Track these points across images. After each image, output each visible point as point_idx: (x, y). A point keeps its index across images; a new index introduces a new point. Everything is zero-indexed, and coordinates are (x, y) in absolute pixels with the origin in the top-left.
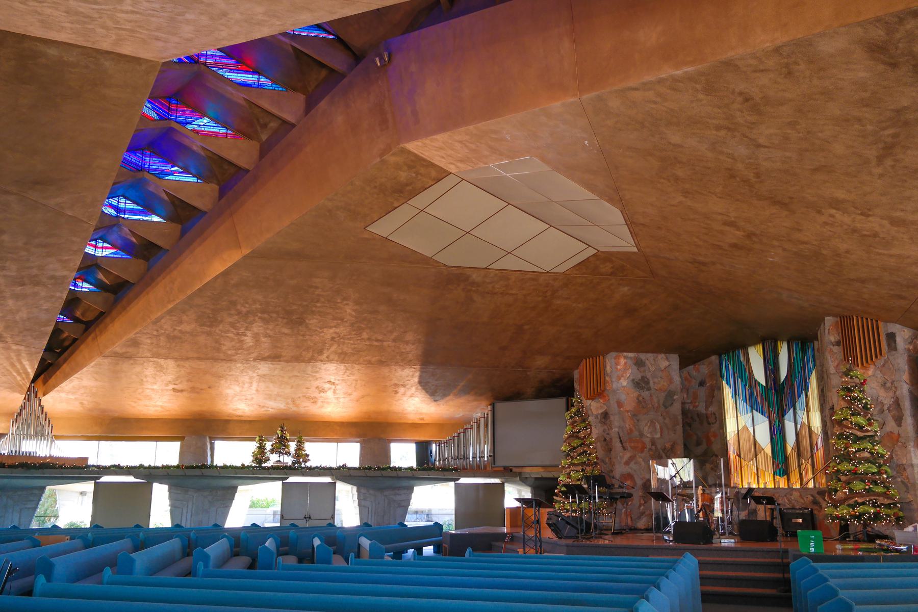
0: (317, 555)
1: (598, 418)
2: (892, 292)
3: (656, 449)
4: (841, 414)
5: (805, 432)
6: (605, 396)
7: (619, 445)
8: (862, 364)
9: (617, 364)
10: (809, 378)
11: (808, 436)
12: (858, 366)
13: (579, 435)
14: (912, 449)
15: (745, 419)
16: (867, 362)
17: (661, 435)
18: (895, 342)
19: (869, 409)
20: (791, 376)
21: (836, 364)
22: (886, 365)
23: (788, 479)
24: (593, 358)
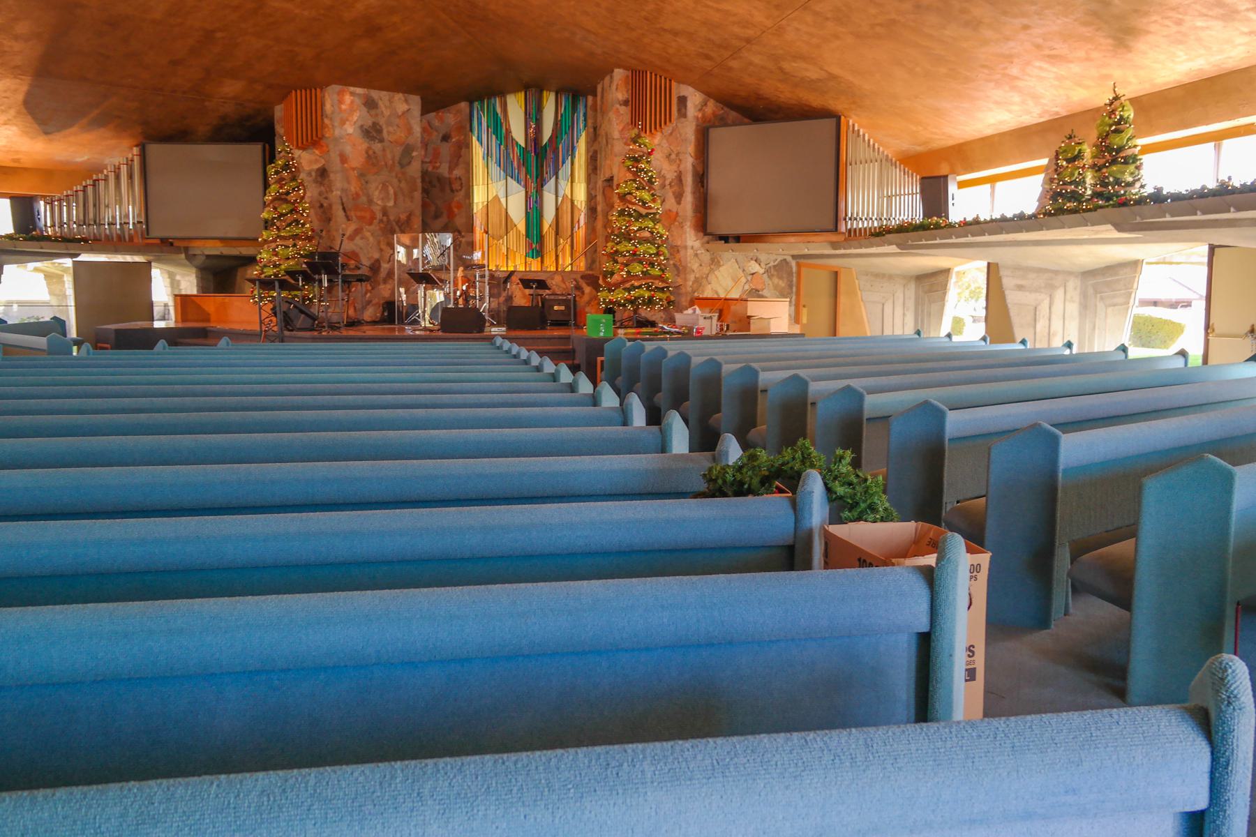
0: (197, 321)
1: (311, 176)
2: (701, 50)
3: (389, 220)
4: (625, 188)
5: (567, 207)
6: (322, 146)
7: (341, 213)
8: (651, 131)
9: (341, 102)
10: (577, 142)
11: (569, 210)
12: (646, 132)
13: (289, 198)
14: (688, 230)
15: (498, 188)
16: (656, 128)
17: (395, 202)
18: (685, 107)
19: (653, 183)
20: (557, 137)
21: (621, 128)
22: (674, 134)
23: (542, 262)
24: (311, 90)
